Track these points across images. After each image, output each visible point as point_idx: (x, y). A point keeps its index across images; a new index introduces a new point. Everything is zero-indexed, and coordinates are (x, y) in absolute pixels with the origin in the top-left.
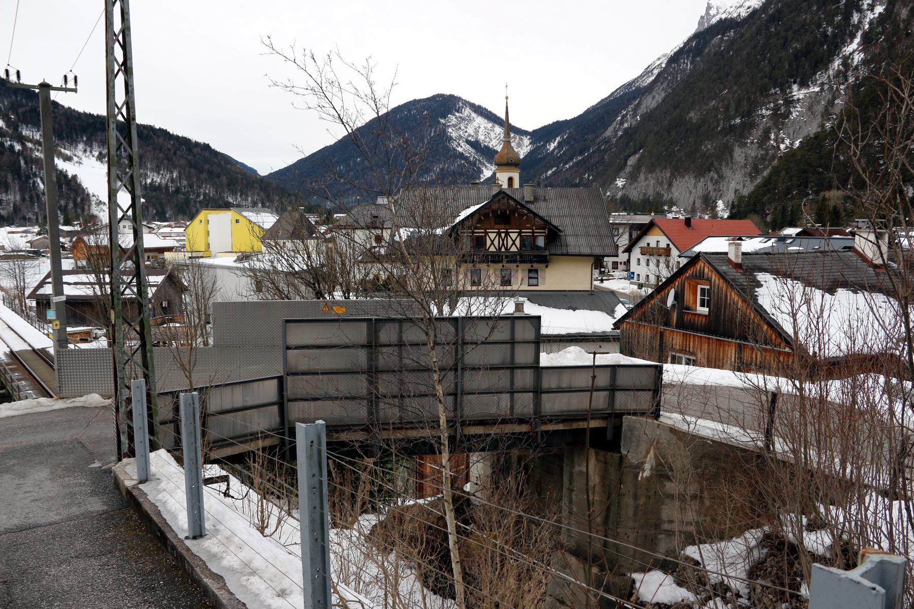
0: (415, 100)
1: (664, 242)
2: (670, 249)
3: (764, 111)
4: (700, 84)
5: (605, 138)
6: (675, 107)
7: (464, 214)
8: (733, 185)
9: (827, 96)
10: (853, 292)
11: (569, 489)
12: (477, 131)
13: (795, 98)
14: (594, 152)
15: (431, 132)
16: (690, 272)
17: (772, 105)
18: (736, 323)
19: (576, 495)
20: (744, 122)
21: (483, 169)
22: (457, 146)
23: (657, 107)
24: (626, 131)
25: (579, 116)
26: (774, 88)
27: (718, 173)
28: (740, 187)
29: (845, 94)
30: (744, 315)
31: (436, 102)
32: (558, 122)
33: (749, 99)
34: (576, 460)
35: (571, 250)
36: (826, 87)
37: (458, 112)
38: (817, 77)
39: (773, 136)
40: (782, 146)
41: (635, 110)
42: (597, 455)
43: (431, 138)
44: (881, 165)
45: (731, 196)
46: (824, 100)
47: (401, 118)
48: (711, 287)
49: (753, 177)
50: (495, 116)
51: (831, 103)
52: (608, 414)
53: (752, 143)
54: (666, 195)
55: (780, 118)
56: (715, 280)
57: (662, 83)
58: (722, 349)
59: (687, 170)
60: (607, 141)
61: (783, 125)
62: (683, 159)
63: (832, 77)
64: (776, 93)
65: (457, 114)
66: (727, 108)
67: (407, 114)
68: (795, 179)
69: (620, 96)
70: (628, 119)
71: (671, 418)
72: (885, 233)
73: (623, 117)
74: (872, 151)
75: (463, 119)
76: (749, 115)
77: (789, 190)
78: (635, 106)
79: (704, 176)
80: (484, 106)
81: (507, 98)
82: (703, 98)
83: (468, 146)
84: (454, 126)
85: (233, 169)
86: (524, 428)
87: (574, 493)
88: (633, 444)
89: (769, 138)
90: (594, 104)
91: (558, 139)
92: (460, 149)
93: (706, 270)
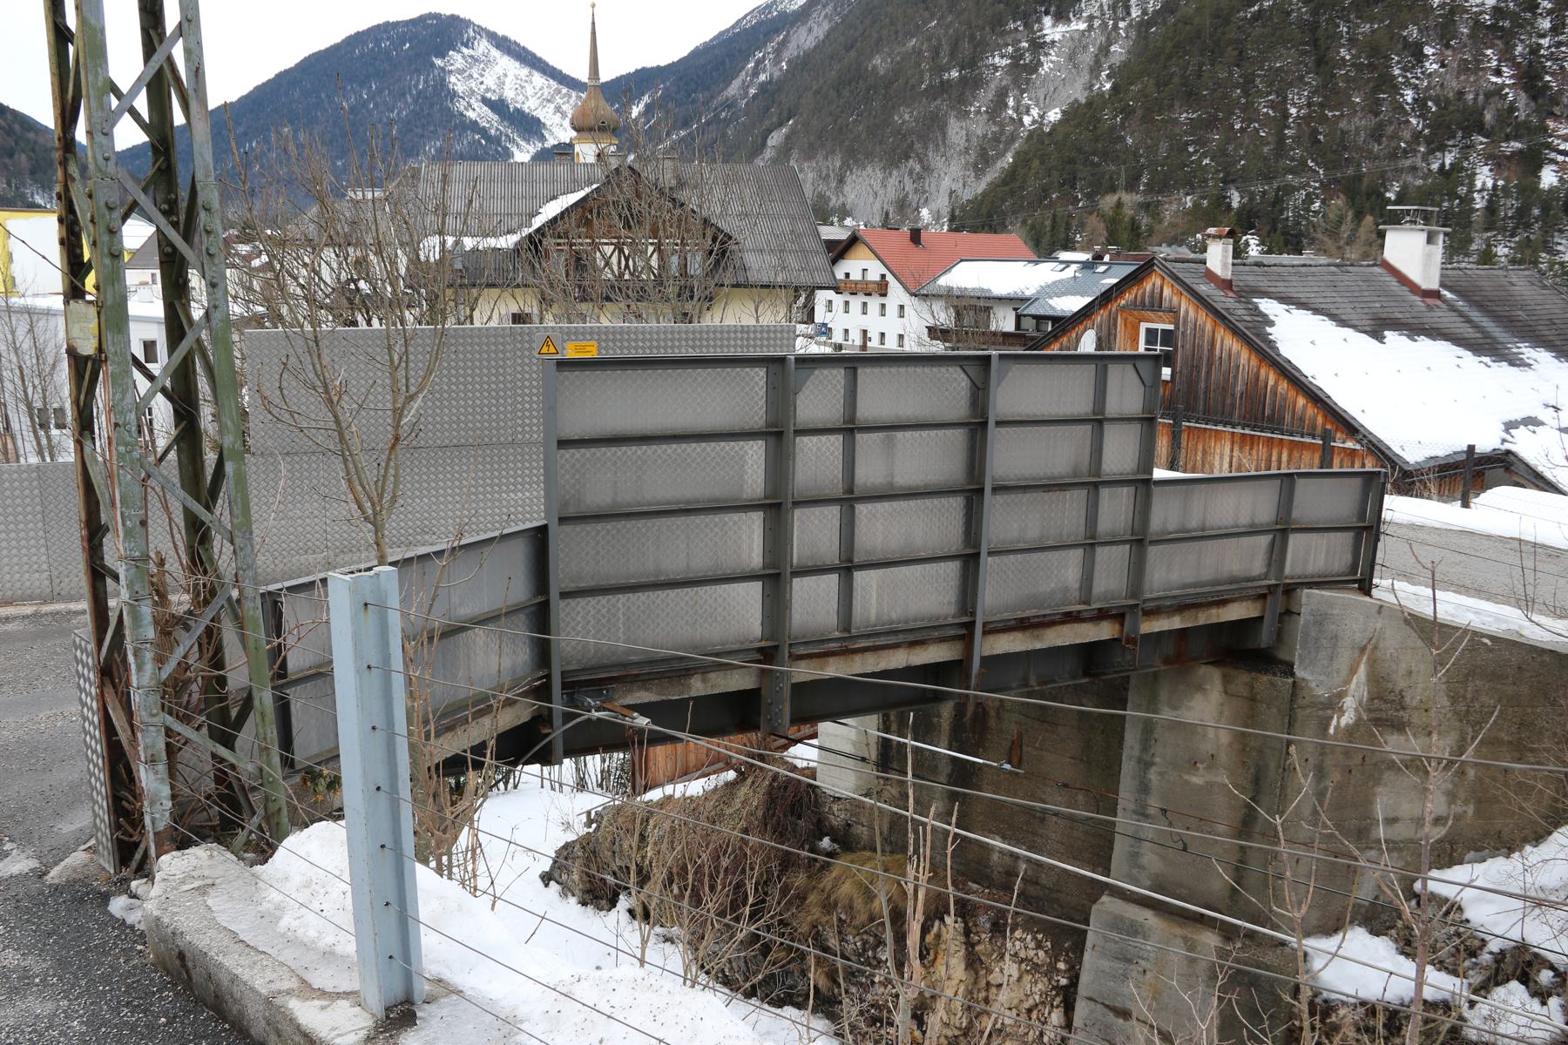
0: (387, 24)
1: (875, 270)
2: (887, 284)
3: (997, 60)
4: (889, 9)
5: (727, 99)
6: (848, 48)
7: (551, 210)
8: (946, 183)
9: (1098, 37)
10: (1408, 337)
11: (1140, 760)
12: (501, 83)
13: (1048, 39)
14: (708, 123)
15: (418, 81)
16: (1129, 297)
17: (1010, 49)
18: (1233, 395)
19: (1161, 774)
20: (965, 77)
21: (514, 149)
22: (466, 109)
23: (816, 47)
24: (763, 87)
25: (681, 61)
26: (1014, 22)
27: (921, 161)
28: (958, 186)
29: (1127, 37)
30: (1255, 382)
31: (426, 27)
32: (644, 69)
33: (972, 37)
34: (1163, 695)
35: (753, 277)
36: (1097, 23)
37: (467, 47)
38: (1083, 5)
39: (1011, 102)
40: (1027, 120)
41: (778, 52)
42: (1226, 680)
43: (419, 93)
44: (1191, 154)
45: (942, 202)
46: (1094, 46)
47: (362, 55)
48: (1177, 327)
49: (979, 170)
50: (534, 55)
51: (1104, 50)
52: (1269, 587)
53: (978, 112)
54: (834, 199)
55: (1023, 71)
56: (1187, 312)
57: (824, 7)
58: (1200, 447)
59: (869, 156)
60: (730, 104)
61: (1027, 84)
62: (863, 136)
63: (1106, 8)
64: (1016, 29)
65: (465, 50)
66: (936, 52)
67: (373, 49)
68: (1055, 173)
69: (752, 27)
70: (767, 67)
71: (1413, 596)
72: (1438, 232)
73: (759, 62)
74: (1177, 130)
75: (476, 60)
76: (971, 63)
77: (1045, 192)
78: (778, 44)
79: (897, 167)
80: (513, 39)
81: (593, 6)
82: (897, 32)
83: (486, 108)
84: (461, 72)
85: (41, 140)
86: (1104, 631)
87: (1154, 769)
88: (1323, 654)
89: (1006, 106)
90: (707, 39)
91: (646, 99)
92: (471, 115)
93: (1167, 292)
